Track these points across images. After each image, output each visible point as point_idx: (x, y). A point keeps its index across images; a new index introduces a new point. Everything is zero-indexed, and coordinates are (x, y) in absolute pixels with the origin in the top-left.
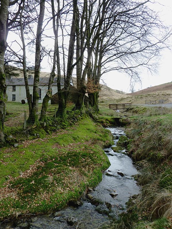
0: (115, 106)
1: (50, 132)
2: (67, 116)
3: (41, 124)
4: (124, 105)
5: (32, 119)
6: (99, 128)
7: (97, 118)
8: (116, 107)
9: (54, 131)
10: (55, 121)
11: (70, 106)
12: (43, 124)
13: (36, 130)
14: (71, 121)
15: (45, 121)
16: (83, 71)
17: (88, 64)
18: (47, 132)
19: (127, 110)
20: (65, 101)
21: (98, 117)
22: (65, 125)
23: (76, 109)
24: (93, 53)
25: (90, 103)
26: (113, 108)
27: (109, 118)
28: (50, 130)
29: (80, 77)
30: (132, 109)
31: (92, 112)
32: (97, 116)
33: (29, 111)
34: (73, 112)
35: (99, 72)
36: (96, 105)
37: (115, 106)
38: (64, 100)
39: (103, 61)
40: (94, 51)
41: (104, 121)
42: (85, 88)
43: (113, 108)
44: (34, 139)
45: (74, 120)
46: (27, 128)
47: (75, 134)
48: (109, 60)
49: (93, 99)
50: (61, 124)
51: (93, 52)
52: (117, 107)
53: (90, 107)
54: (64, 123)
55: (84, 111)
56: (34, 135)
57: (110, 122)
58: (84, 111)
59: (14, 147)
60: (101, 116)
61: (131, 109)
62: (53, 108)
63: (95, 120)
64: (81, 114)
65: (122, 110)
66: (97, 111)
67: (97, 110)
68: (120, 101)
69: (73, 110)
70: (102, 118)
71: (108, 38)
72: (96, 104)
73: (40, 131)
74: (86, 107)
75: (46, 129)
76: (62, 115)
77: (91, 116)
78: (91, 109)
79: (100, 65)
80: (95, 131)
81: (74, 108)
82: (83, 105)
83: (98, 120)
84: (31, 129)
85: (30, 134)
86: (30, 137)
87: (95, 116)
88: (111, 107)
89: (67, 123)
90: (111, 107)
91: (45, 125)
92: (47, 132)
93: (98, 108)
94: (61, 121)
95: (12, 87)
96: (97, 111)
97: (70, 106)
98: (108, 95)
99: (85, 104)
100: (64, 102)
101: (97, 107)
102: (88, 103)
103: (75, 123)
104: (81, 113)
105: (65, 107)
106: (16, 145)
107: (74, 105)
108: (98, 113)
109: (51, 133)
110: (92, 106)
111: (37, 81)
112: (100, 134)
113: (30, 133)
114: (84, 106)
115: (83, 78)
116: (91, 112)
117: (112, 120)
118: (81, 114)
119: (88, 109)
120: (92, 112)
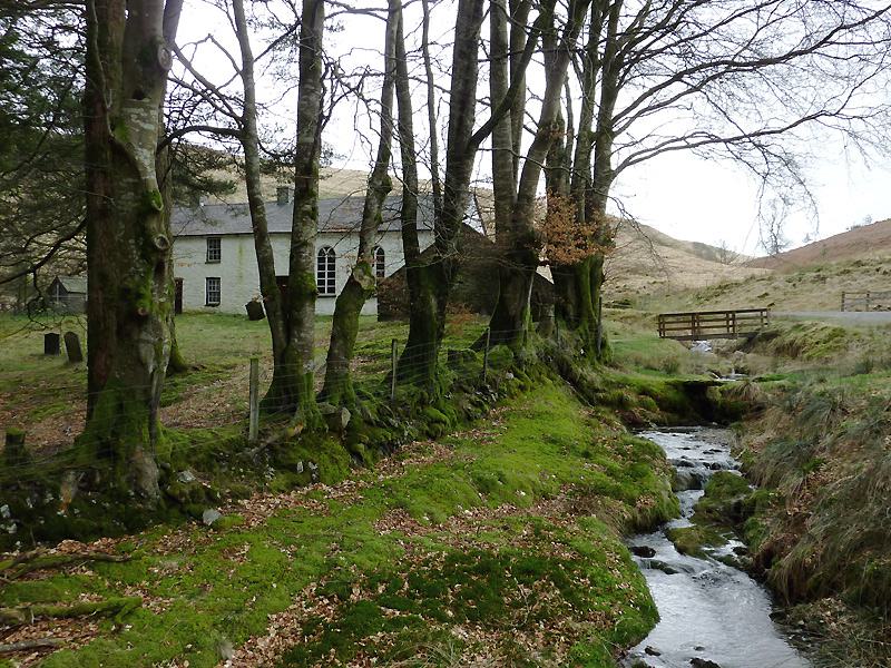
1: (367, 456)
3: (327, 416)
4: (730, 316)
6: (604, 433)
7: (598, 385)
9: (390, 447)
11: (464, 328)
12: (338, 415)
13: (303, 444)
14: (472, 403)
15: (345, 402)
18: (356, 454)
19: (750, 340)
20: (441, 305)
21: (599, 379)
22: (439, 421)
24: (570, 69)
25: (561, 312)
27: (657, 381)
30: (774, 335)
32: (594, 374)
34: (479, 356)
35: (603, 161)
36: (591, 320)
38: (433, 302)
41: (632, 398)
45: (482, 395)
46: (262, 434)
47: (489, 462)
50: (419, 416)
53: (564, 333)
54: (434, 412)
55: (530, 351)
56: (293, 468)
60: (613, 375)
61: (769, 337)
63: (585, 393)
66: (597, 352)
67: (596, 347)
70: (621, 385)
74: (543, 330)
75: (349, 437)
76: (424, 370)
77: (566, 373)
78: (565, 339)
79: (606, 133)
80: (583, 447)
81: (486, 335)
82: (528, 323)
83: (600, 395)
87: (591, 374)
88: (667, 326)
90: (667, 326)
91: (346, 418)
92: (356, 454)
94: (422, 402)
96: (597, 352)
97: (464, 328)
101: (595, 328)
102: (552, 314)
103: (487, 407)
104: (519, 362)
106: (211, 515)
108: (599, 359)
109: (375, 458)
110: (573, 325)
112: (610, 462)
117: (671, 394)
119: (553, 342)
120: (573, 353)
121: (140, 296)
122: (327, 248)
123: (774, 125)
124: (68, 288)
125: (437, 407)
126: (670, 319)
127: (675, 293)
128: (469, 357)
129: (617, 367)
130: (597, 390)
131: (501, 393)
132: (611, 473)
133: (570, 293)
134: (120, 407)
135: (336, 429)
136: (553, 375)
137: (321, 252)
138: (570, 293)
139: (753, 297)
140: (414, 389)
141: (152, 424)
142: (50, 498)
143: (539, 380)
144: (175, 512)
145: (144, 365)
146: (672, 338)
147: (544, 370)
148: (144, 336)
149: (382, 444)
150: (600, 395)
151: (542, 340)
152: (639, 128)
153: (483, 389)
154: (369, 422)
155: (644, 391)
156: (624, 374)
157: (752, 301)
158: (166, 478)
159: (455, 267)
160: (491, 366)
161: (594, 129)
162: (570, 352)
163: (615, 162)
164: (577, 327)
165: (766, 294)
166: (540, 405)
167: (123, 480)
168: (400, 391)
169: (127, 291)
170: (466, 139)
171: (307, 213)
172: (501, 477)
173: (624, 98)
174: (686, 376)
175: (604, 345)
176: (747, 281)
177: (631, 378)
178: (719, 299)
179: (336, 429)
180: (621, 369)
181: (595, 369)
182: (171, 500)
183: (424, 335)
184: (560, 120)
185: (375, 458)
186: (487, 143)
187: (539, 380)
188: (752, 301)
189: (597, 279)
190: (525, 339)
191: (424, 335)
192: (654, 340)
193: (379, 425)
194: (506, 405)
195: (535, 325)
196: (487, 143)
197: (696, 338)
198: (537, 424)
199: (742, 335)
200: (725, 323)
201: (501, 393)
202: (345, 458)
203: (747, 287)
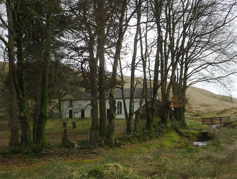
0: (209, 121)
1: (141, 141)
2: (154, 129)
3: (135, 134)
4: (220, 119)
5: (128, 130)
6: (183, 140)
7: (184, 133)
8: (211, 122)
9: (144, 140)
10: (145, 133)
11: (156, 120)
12: (137, 134)
13: (132, 138)
14: (158, 134)
15: (137, 132)
16: (167, 86)
17: (173, 77)
18: (140, 141)
19: (226, 124)
20: (152, 116)
21: (184, 132)
22: (152, 137)
23: (162, 123)
24: (178, 64)
25: (176, 117)
26: (206, 123)
27: (196, 132)
28: (141, 140)
29: (165, 93)
30: (231, 123)
31: (178, 126)
32: (183, 131)
33: (126, 124)
34: (159, 126)
35: (185, 83)
36: (182, 119)
37: (209, 121)
38: (151, 115)
39: (188, 73)
40: (179, 63)
41: (191, 136)
42: (170, 103)
43: (206, 123)
44: (132, 144)
45: (160, 133)
46: (126, 136)
47: (162, 143)
48: (196, 71)
49: (179, 113)
50: (149, 136)
51: (178, 63)
52: (221, 121)
53: (176, 122)
54: (151, 135)
55: (169, 125)
56: (131, 141)
57: (197, 137)
58: (169, 125)
59: (121, 147)
60: (187, 131)
61: (229, 124)
62: (143, 122)
63: (180, 134)
64: (167, 128)
65: (220, 125)
66: (184, 126)
67: (184, 125)
68: (222, 114)
69: (159, 124)
70: (189, 133)
71: (194, 48)
72: (182, 118)
73: (134, 139)
74: (172, 121)
75: (138, 138)
76: (149, 128)
77: (177, 130)
78: (177, 123)
79: (186, 78)
80: (178, 142)
81: (160, 122)
82: (168, 120)
83: (184, 135)
84: (129, 137)
85: (129, 141)
86: (129, 143)
87: (182, 130)
88: (204, 121)
89: (154, 135)
90: (204, 121)
91: (138, 135)
92: (140, 141)
93: (185, 122)
94: (149, 133)
95: (69, 102)
96: (184, 126)
97: (156, 120)
98: (208, 105)
99: (171, 118)
100: (151, 117)
101: (183, 121)
102: (174, 118)
103: (161, 135)
104: (167, 127)
105: (152, 121)
106: (122, 146)
107: (160, 120)
108: (184, 127)
109: (142, 142)
110: (178, 120)
111: (132, 102)
112: (183, 144)
113: (129, 140)
114: (170, 120)
115: (168, 94)
116: (177, 127)
117: (199, 135)
118: (167, 128)
119: (174, 124)
120: (178, 126)
121: (113, 115)
122: (120, 102)
123: (223, 76)
124: (54, 112)
125: (152, 134)
126: (214, 119)
127: (212, 112)
128: (157, 126)
129: (188, 130)
130: (183, 134)
131: (163, 133)
132: (182, 145)
133: (178, 113)
134: (109, 131)
135: (136, 136)
136: (174, 130)
137: (118, 103)
138: (178, 113)
139: (232, 113)
140: (148, 131)
141: (113, 133)
142: (101, 143)
143: (171, 131)
144: (117, 146)
145: (113, 125)
146: (205, 124)
147: (172, 129)
148: (113, 120)
149: (143, 139)
150: (184, 135)
151: (171, 123)
152: (192, 77)
153: (160, 132)
154: (141, 136)
155: (193, 134)
156: (190, 131)
157: (232, 114)
158: (115, 141)
159: (154, 109)
160: (161, 128)
161: (183, 78)
162: (177, 126)
163: (188, 84)
164: (180, 120)
165: (236, 112)
166: (171, 135)
167: (110, 141)
168: (146, 131)
169: (111, 114)
170: (157, 86)
171: (132, 101)
172: (164, 145)
173: (190, 70)
174: (204, 131)
175: (185, 124)
176: (231, 109)
177: (191, 131)
178: (223, 114)
179: (136, 136)
180: (189, 130)
181: (183, 130)
182: (116, 144)
183: (149, 121)
184: (175, 76)
185: (142, 142)
186: (160, 87)
187: (171, 131)
188: (232, 114)
189: (184, 110)
190: (168, 123)
191: (149, 121)
192: (201, 124)
193: (143, 136)
194: (164, 135)
195: (170, 120)
196: (160, 87)
197: (212, 124)
198: (170, 138)
199: (223, 123)
200: (219, 120)
201: (163, 133)
202: (138, 141)
203: (231, 111)
